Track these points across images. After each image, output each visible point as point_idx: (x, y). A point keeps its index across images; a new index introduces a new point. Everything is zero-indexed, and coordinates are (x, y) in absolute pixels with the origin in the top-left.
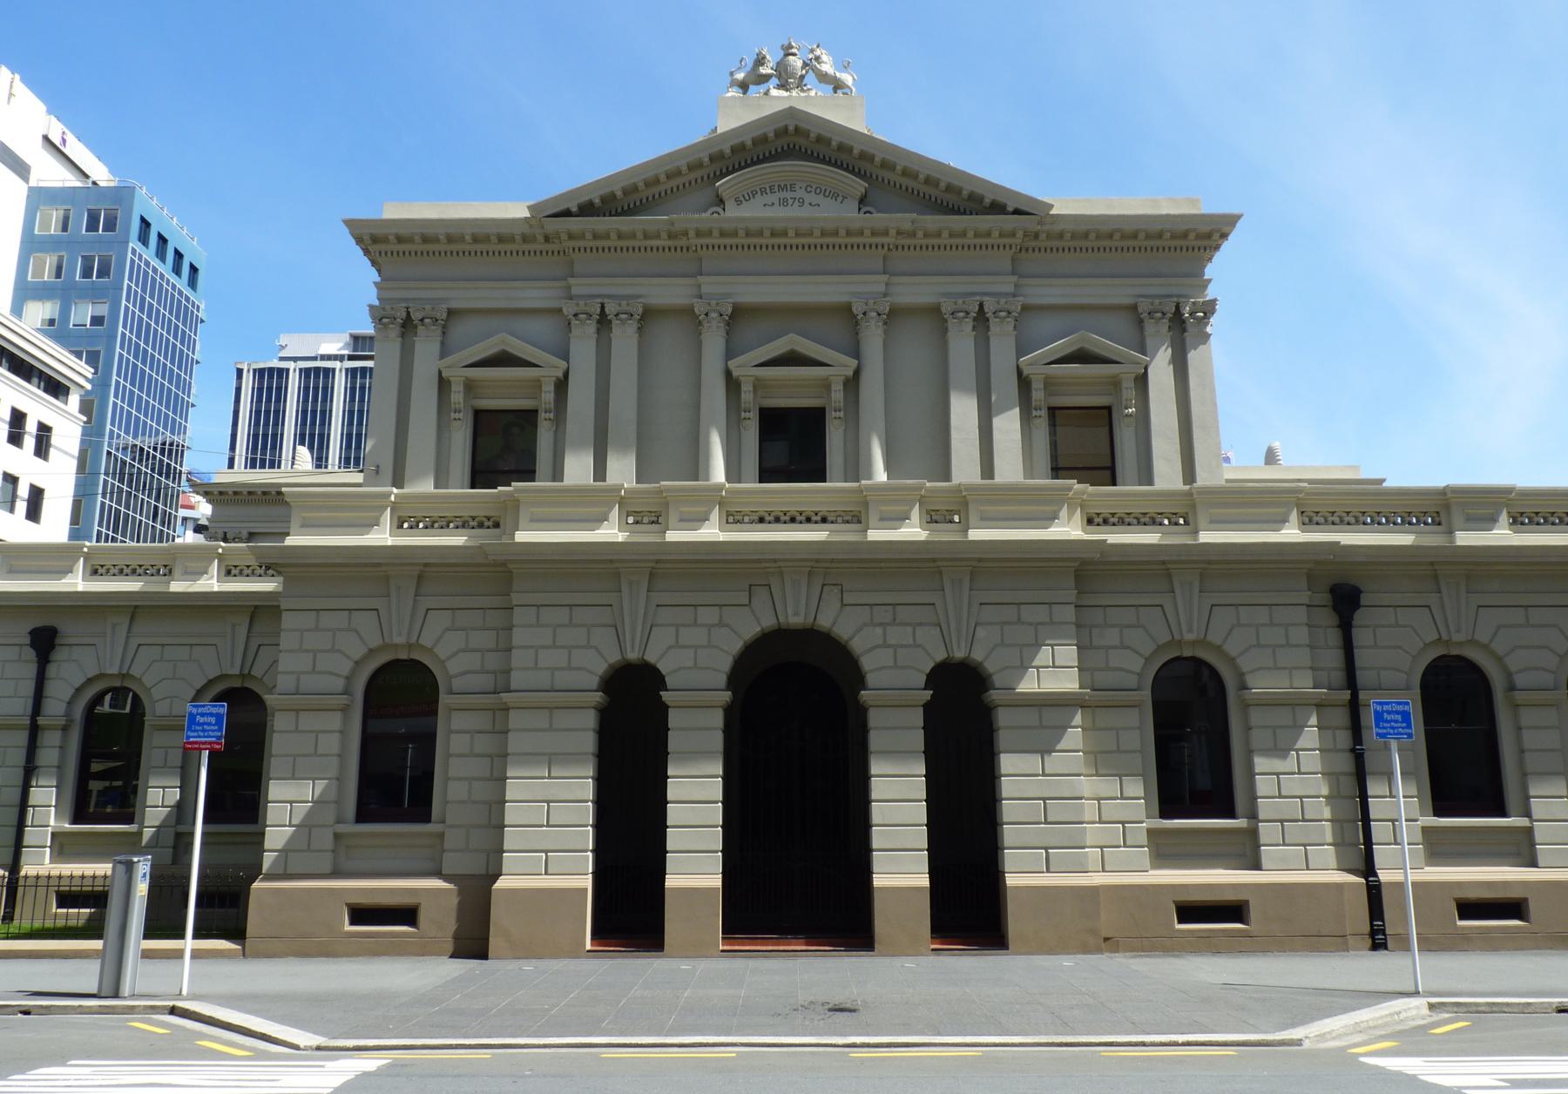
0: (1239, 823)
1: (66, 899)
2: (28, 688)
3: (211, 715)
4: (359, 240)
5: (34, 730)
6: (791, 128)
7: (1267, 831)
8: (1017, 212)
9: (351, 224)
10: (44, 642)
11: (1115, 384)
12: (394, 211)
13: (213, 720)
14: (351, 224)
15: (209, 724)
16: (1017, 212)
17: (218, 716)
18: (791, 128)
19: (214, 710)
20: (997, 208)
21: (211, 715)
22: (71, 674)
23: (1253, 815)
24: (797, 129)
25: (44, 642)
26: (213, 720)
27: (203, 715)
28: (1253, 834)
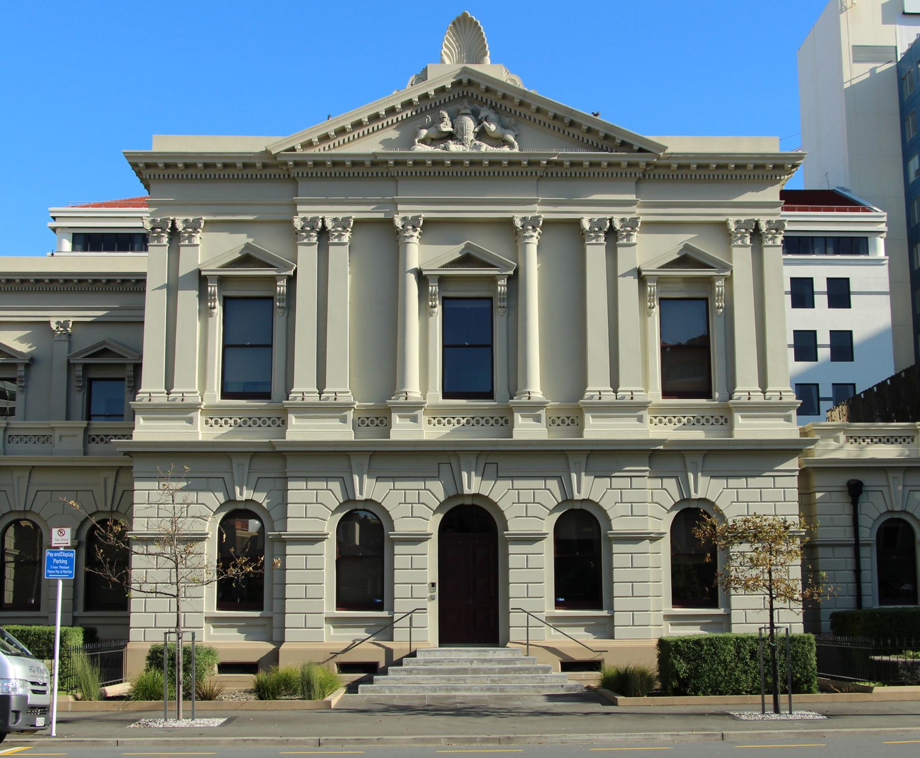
0: (604, 613)
1: (569, 666)
2: (848, 520)
3: (64, 558)
4: (134, 166)
5: (857, 546)
6: (465, 81)
7: (618, 618)
8: (641, 150)
9: (128, 156)
10: (855, 491)
11: (709, 281)
12: (166, 144)
13: (66, 562)
14: (128, 156)
15: (63, 565)
16: (641, 150)
17: (69, 559)
18: (465, 81)
19: (67, 555)
20: (625, 145)
21: (64, 558)
22: (873, 510)
23: (611, 608)
24: (470, 82)
25: (855, 491)
26: (66, 562)
27: (58, 558)
28: (728, 616)
